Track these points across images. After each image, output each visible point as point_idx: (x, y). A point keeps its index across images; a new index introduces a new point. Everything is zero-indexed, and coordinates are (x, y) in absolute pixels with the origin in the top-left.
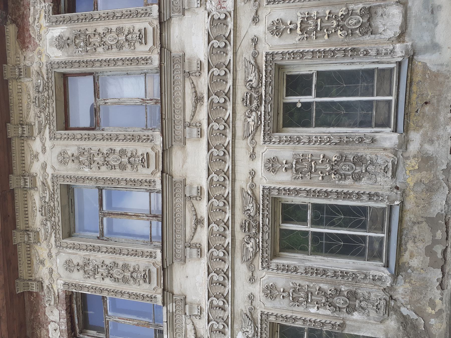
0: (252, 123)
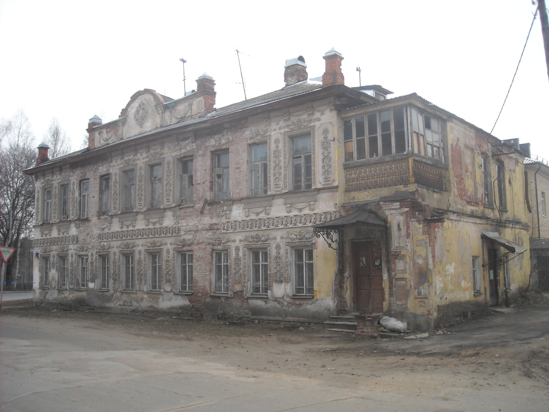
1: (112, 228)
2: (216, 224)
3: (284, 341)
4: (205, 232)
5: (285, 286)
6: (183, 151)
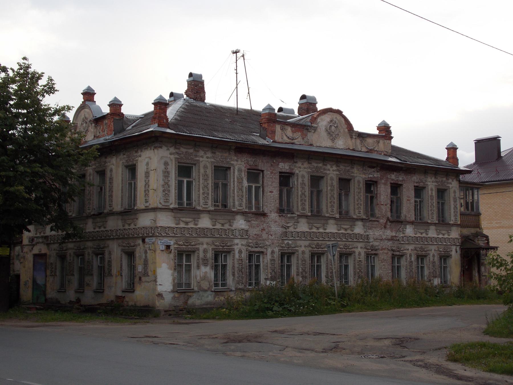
0: (217, 244)
2: (395, 236)
3: (174, 323)
5: (438, 279)
6: (372, 176)
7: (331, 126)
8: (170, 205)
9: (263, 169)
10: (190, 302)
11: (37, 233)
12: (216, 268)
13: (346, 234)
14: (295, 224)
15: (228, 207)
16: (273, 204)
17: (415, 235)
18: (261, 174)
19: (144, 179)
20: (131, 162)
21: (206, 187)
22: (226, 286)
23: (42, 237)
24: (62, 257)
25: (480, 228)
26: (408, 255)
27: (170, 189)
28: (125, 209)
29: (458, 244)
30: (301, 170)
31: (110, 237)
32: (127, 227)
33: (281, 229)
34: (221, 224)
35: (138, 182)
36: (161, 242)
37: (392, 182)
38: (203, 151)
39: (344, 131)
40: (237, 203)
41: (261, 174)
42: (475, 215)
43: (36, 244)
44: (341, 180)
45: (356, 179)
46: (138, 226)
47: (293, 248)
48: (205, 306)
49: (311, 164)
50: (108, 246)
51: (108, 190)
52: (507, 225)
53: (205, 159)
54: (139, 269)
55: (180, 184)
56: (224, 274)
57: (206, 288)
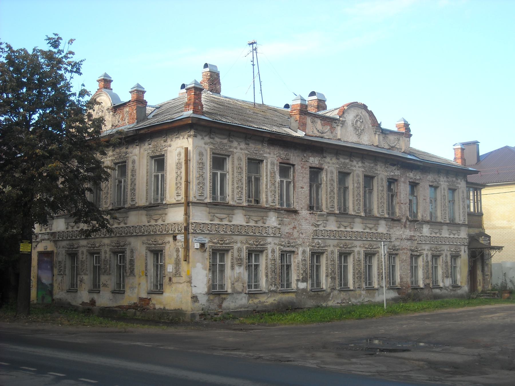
1: (327, 226)
2: (414, 236)
4: (406, 241)
6: (392, 174)
7: (357, 121)
8: (205, 199)
9: (294, 163)
10: (225, 304)
11: (68, 227)
12: (249, 267)
13: (370, 233)
14: (324, 222)
15: (261, 203)
16: (304, 201)
17: (430, 235)
18: (292, 168)
19: (175, 170)
20: (159, 153)
21: (240, 180)
22: (259, 288)
23: (48, 233)
24: (73, 255)
25: (484, 229)
26: (425, 255)
27: (205, 181)
28: (151, 203)
29: (466, 244)
30: (330, 165)
31: (132, 233)
32: (153, 223)
33: (311, 227)
34: (254, 221)
35: (168, 174)
36: (195, 240)
37: (410, 181)
38: (237, 141)
39: (369, 127)
40: (270, 199)
41: (292, 168)
42: (478, 215)
43: (41, 241)
44: (366, 176)
45: (380, 177)
46: (166, 222)
47: (322, 247)
48: (239, 310)
49: (339, 159)
50: (130, 244)
51: (129, 182)
52: (492, 226)
53: (238, 150)
54: (168, 269)
55: (214, 175)
56: (256, 275)
57: (240, 290)
